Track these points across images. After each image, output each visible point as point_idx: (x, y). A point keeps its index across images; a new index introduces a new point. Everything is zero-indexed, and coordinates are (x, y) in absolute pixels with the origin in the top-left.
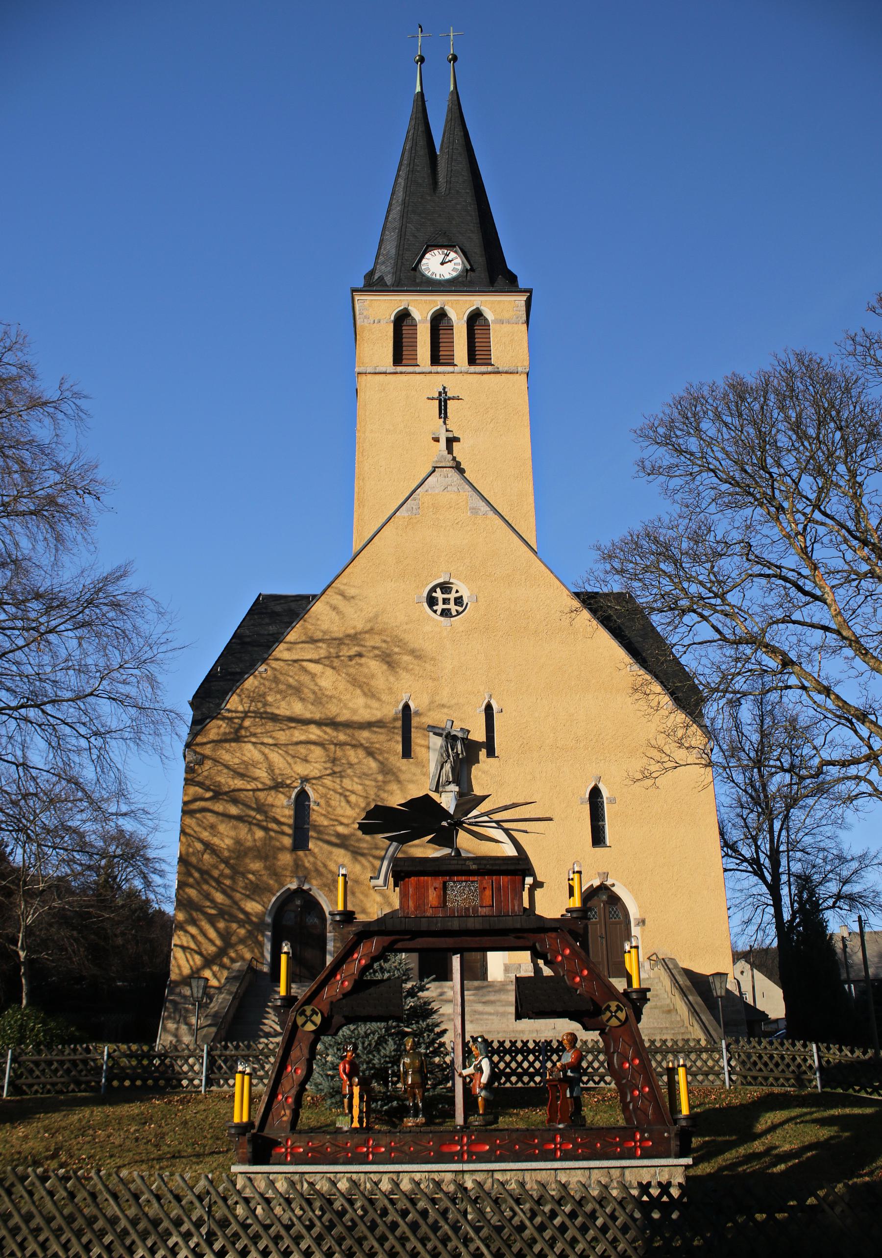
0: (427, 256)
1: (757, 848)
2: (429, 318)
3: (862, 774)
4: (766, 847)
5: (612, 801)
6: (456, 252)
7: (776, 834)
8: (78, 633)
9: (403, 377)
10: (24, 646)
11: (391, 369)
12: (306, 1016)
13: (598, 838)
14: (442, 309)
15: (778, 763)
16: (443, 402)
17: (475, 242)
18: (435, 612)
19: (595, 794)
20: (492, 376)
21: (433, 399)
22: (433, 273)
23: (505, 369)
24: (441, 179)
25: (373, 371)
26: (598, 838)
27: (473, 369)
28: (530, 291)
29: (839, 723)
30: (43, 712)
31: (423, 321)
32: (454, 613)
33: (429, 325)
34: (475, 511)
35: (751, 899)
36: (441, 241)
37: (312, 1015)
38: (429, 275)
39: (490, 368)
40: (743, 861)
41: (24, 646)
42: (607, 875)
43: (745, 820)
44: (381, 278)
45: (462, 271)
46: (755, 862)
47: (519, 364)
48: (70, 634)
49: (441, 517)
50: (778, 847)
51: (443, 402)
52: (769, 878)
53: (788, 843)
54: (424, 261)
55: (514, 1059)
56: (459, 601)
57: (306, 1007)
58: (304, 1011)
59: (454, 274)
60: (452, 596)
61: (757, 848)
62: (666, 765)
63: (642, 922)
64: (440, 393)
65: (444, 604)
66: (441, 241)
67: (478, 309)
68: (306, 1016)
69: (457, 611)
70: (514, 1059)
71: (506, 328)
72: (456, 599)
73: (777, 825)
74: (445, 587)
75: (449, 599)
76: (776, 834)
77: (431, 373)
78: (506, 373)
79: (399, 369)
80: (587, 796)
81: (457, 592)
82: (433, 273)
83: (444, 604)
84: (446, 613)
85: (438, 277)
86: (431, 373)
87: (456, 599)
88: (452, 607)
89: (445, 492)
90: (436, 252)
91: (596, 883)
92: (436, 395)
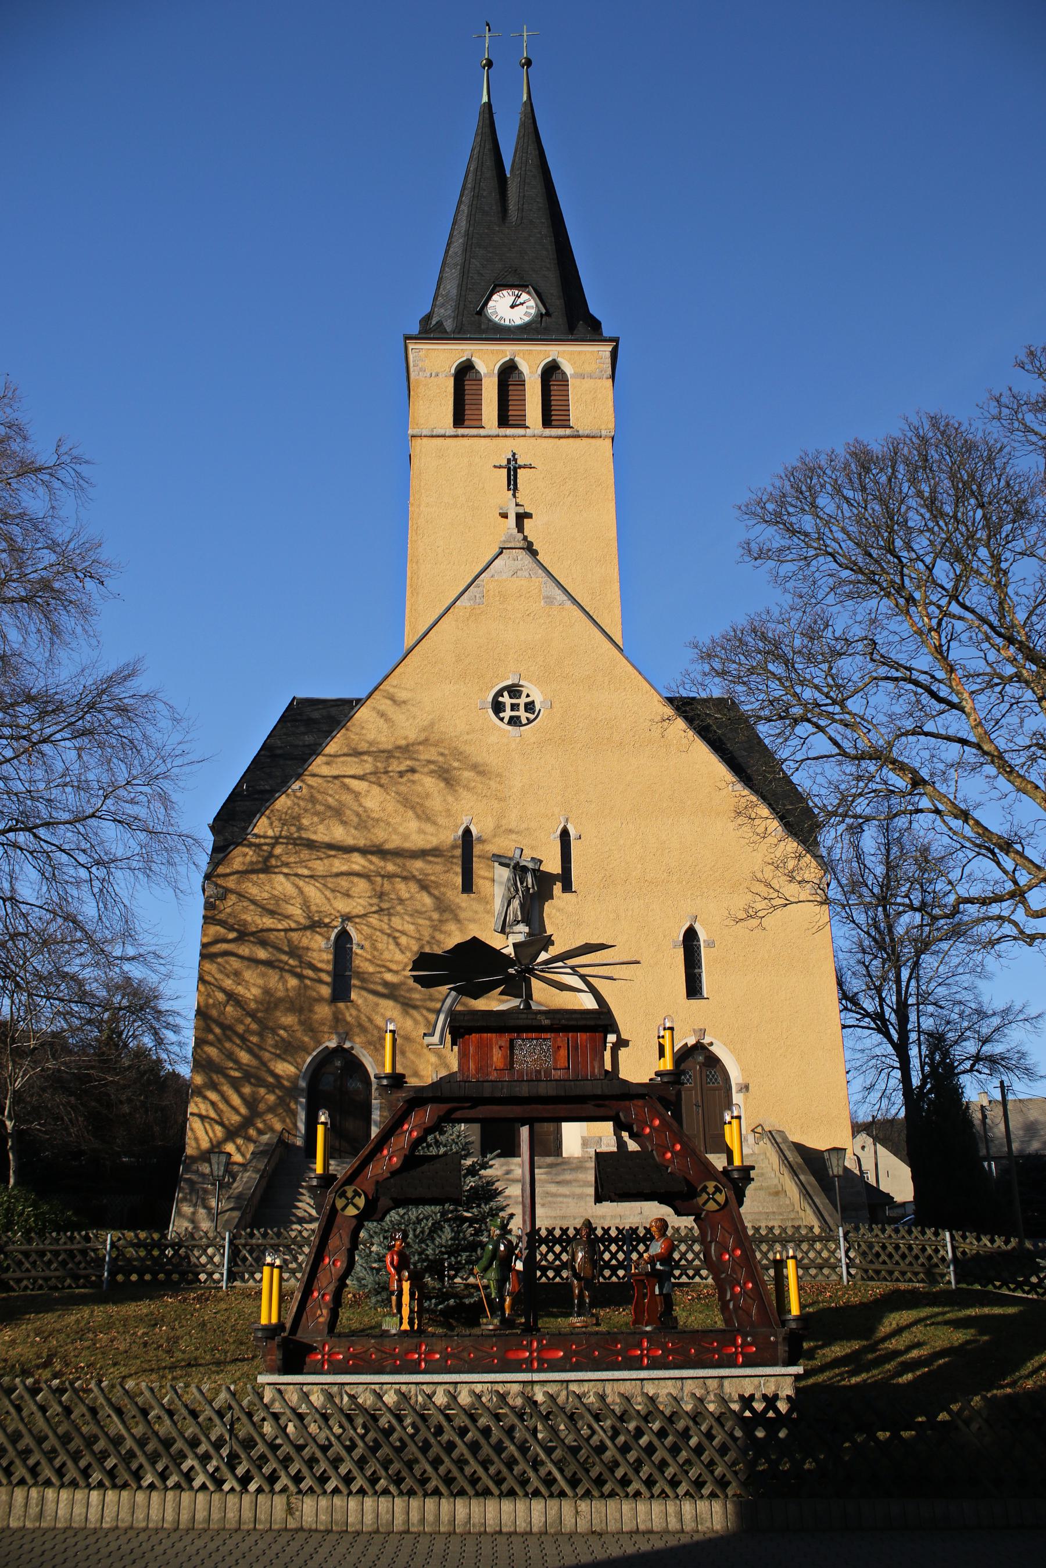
0: (495, 297)
1: (882, 1000)
2: (496, 371)
3: (1005, 914)
4: (892, 999)
5: (711, 944)
6: (528, 293)
7: (904, 984)
8: (78, 742)
9: (464, 441)
10: (13, 759)
11: (452, 431)
12: (347, 1198)
13: (694, 989)
14: (512, 361)
15: (907, 901)
16: (512, 470)
17: (553, 289)
18: (502, 719)
19: (691, 935)
20: (571, 440)
21: (500, 467)
22: (501, 318)
23: (586, 432)
24: (512, 205)
25: (429, 434)
26: (694, 989)
27: (548, 432)
28: (616, 340)
29: (979, 854)
30: (35, 836)
31: (489, 375)
32: (524, 721)
33: (496, 380)
34: (549, 600)
35: (874, 1061)
36: (511, 280)
37: (354, 1197)
38: (497, 319)
39: (568, 431)
40: (864, 1016)
41: (13, 759)
42: (703, 1032)
43: (867, 967)
44: (440, 324)
45: (536, 316)
46: (879, 1017)
47: (603, 427)
48: (68, 744)
49: (509, 608)
50: (906, 999)
51: (512, 470)
52: (895, 1036)
53: (918, 995)
54: (491, 304)
55: (551, 1249)
56: (530, 707)
57: (346, 1188)
58: (345, 1192)
59: (527, 319)
60: (522, 701)
61: (882, 1000)
62: (774, 902)
63: (745, 1088)
64: (509, 460)
65: (512, 710)
66: (511, 280)
67: (554, 360)
68: (347, 1198)
69: (528, 719)
70: (551, 1249)
71: (588, 383)
72: (526, 704)
73: (905, 974)
74: (514, 691)
75: (518, 705)
76: (904, 984)
77: (498, 436)
78: (588, 437)
79: (461, 431)
80: (681, 938)
81: (528, 696)
82: (501, 318)
83: (512, 710)
84: (514, 721)
85: (507, 323)
86: (498, 436)
87: (526, 704)
88: (522, 714)
89: (514, 578)
90: (505, 292)
91: (691, 1041)
92: (504, 463)
